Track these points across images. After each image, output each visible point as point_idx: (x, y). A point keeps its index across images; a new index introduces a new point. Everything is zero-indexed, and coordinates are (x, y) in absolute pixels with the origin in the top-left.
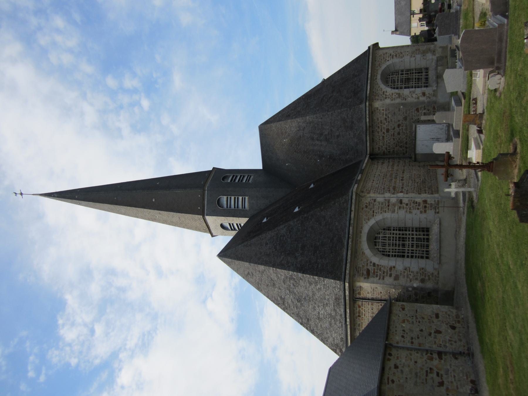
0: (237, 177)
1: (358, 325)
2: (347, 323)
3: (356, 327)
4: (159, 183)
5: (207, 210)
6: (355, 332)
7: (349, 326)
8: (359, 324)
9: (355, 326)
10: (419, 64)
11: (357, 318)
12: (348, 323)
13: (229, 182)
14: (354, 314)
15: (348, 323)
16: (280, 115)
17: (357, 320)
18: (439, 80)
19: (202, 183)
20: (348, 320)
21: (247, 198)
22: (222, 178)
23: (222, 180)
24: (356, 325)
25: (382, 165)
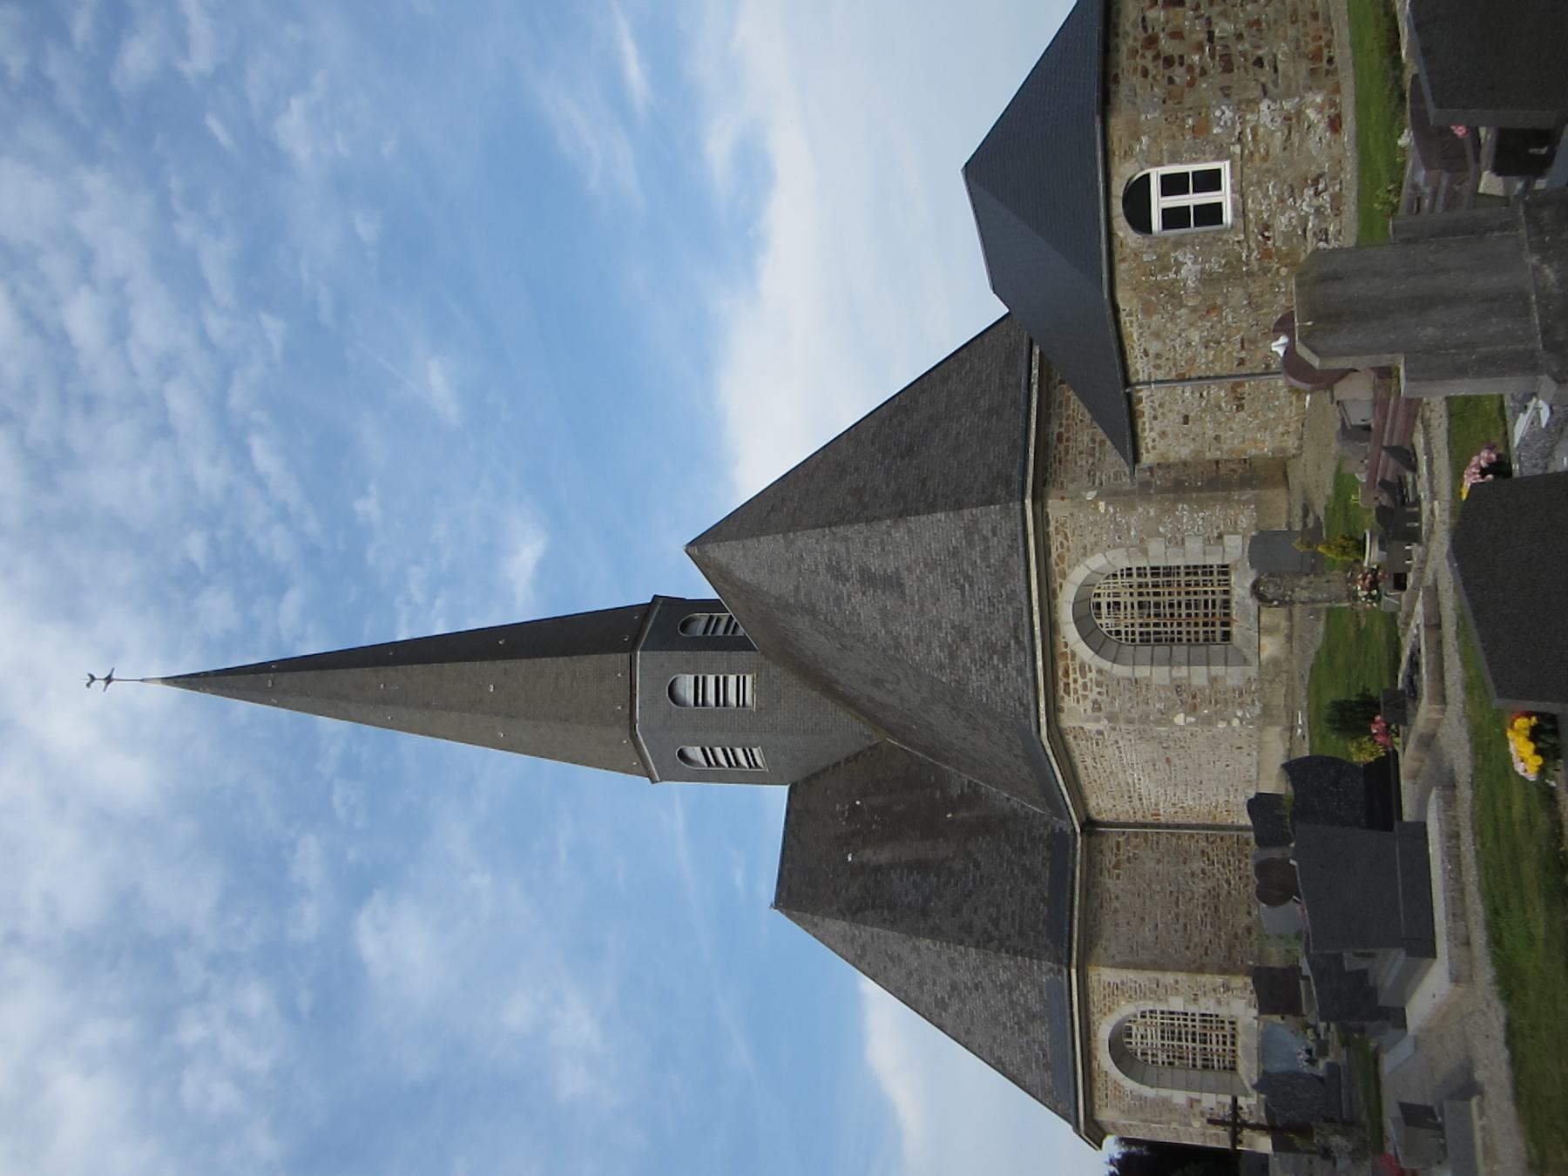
0: (719, 620)
1: (1056, 406)
2: (1032, 380)
3: (1052, 411)
4: (499, 733)
5: (640, 708)
6: (1050, 423)
7: (1035, 387)
8: (1061, 403)
9: (1049, 408)
10: (1434, 996)
11: (1055, 388)
12: (1034, 380)
13: (699, 637)
14: (1050, 379)
15: (1034, 380)
16: (784, 894)
17: (1056, 395)
18: (1433, 621)
19: (636, 617)
20: (1035, 372)
21: (749, 679)
22: (680, 623)
23: (680, 632)
24: (1052, 405)
25: (1196, 1004)
